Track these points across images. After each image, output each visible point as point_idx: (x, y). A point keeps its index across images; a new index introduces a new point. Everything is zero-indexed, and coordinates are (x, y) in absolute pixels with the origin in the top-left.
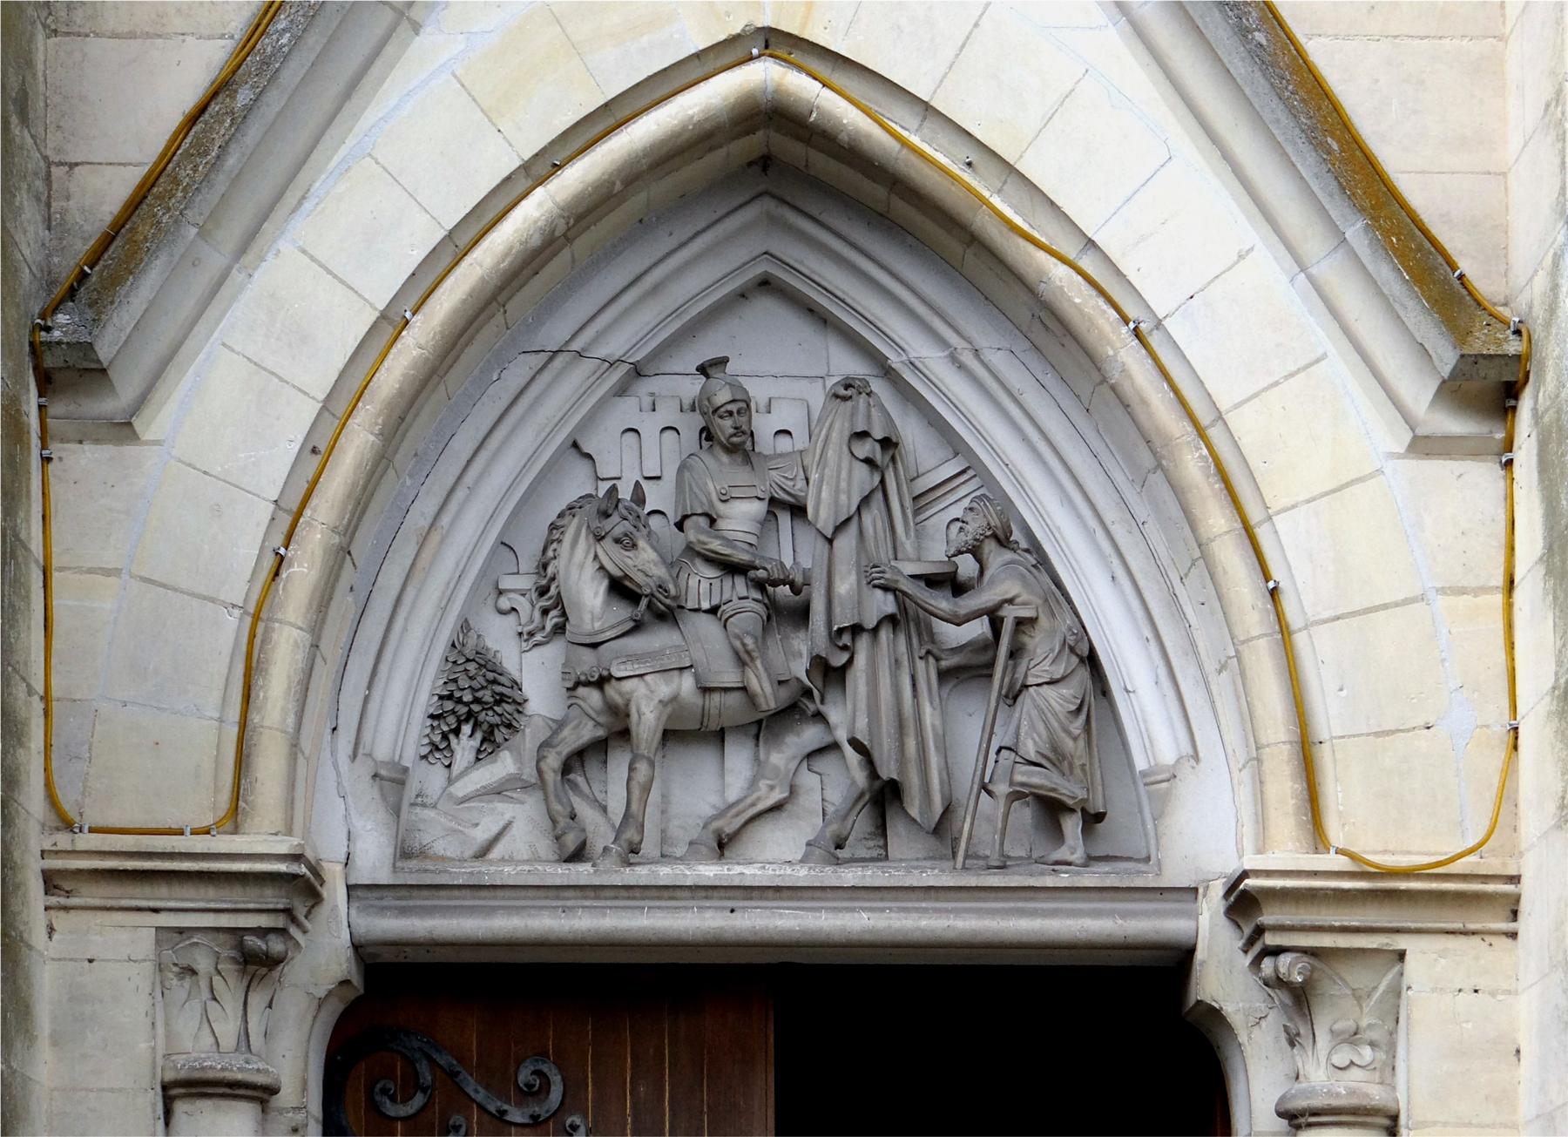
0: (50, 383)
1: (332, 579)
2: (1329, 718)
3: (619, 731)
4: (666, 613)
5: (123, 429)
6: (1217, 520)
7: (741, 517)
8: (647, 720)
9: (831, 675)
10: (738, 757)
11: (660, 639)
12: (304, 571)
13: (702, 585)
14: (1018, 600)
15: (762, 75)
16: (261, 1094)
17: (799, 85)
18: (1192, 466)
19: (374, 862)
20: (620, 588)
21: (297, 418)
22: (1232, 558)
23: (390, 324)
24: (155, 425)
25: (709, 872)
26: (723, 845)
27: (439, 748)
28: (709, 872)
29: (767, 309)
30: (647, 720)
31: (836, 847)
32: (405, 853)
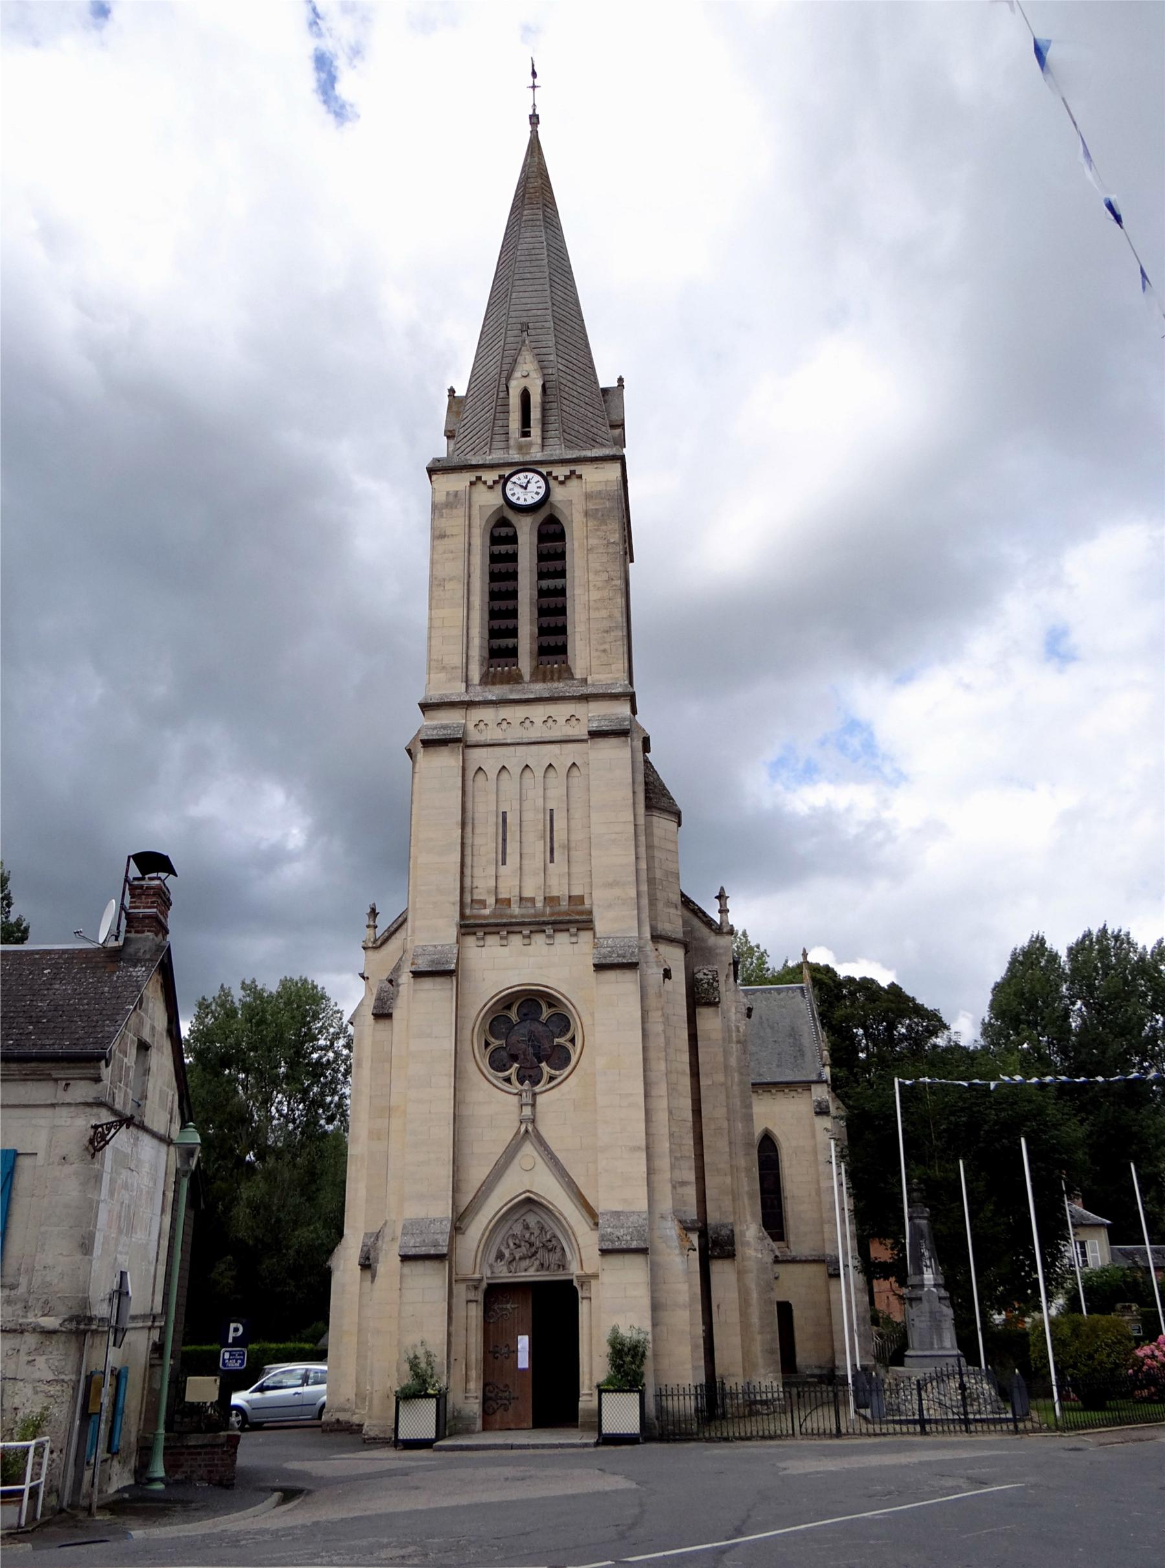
0: (361, 1426)
1: (642, 850)
2: (583, 1258)
3: (514, 1259)
4: (519, 1246)
5: (463, 1234)
6: (572, 1238)
7: (527, 1236)
8: (517, 1258)
9: (536, 1252)
10: (527, 1260)
11: (519, 1250)
12: (483, 1241)
13: (523, 1243)
14: (662, 824)
15: (528, 1194)
16: (476, 1301)
17: (532, 1196)
18: (570, 1232)
19: (489, 1275)
20: (515, 1244)
21: (481, 1232)
22: (574, 1241)
23: (491, 1221)
24: (467, 1233)
25: (524, 1274)
26: (526, 1270)
27: (496, 1261)
28: (524, 1274)
29: (531, 1213)
30: (517, 1258)
31: (537, 1270)
32: (492, 1273)
